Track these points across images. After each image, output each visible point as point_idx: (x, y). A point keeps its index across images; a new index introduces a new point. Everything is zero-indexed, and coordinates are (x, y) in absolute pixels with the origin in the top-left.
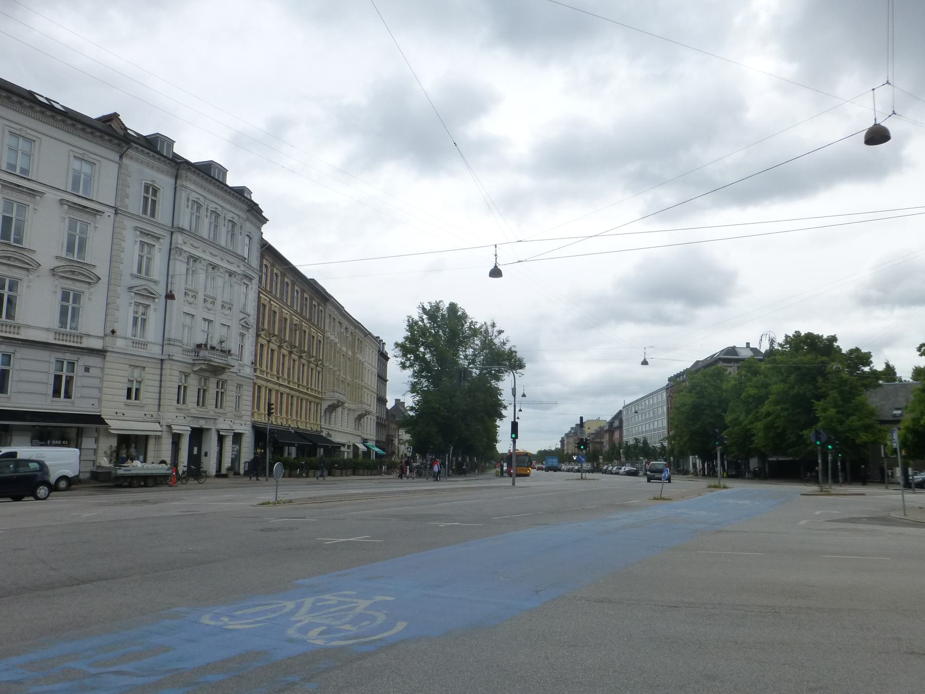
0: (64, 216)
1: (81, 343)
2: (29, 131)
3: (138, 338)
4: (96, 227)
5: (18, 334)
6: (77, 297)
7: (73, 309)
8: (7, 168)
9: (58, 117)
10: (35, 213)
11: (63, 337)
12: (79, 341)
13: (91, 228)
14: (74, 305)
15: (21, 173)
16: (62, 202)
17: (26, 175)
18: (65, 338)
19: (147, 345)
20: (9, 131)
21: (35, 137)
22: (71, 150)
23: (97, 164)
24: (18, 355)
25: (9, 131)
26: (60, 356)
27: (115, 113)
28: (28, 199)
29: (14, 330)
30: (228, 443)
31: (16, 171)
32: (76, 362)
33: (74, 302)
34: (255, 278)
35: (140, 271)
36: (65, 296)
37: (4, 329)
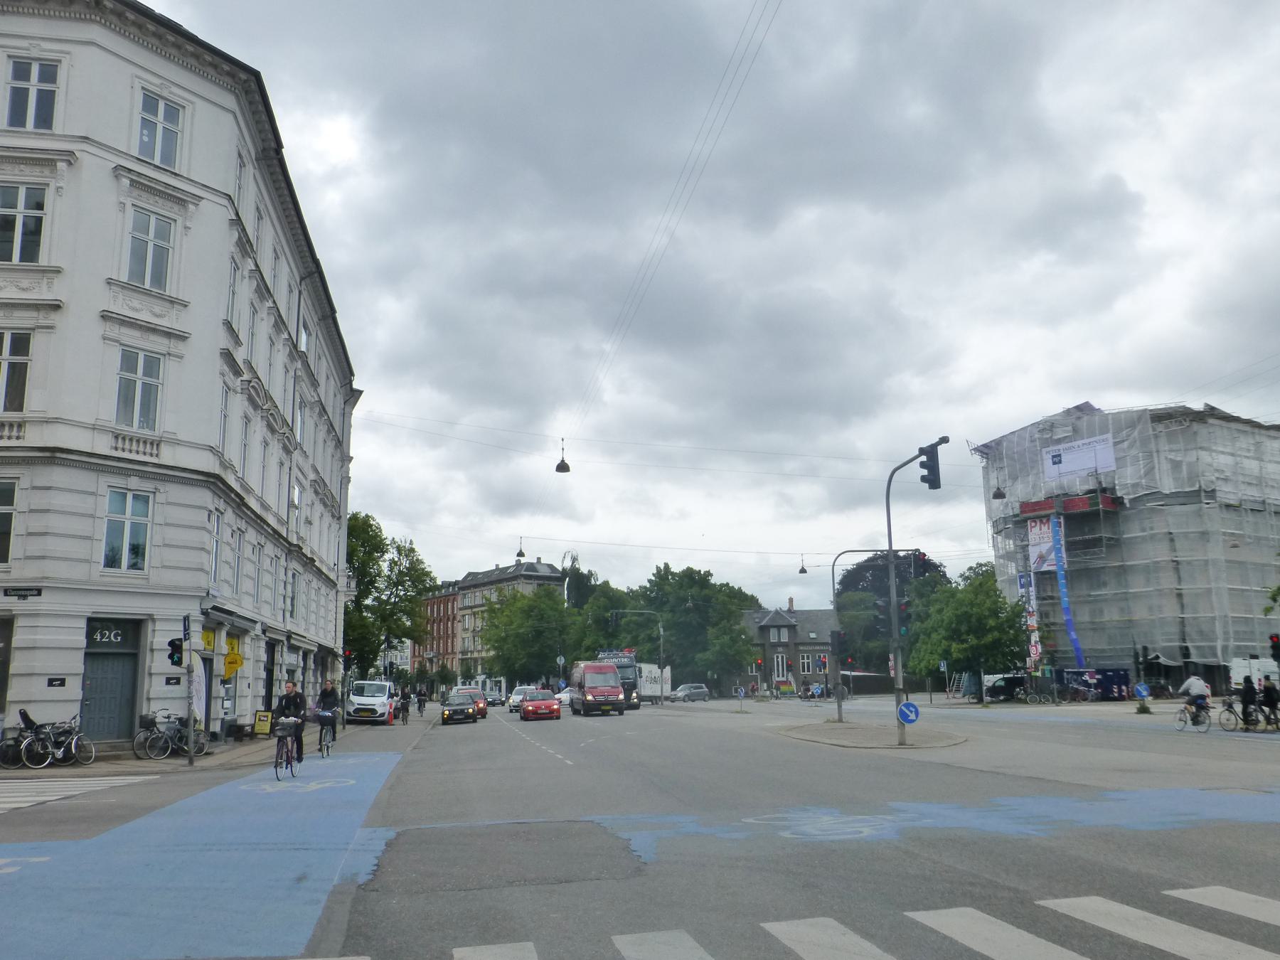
0: (122, 199)
1: (157, 456)
2: (175, 89)
3: (135, 429)
4: (186, 228)
5: (18, 438)
6: (152, 366)
7: (146, 386)
8: (139, 154)
9: (188, 47)
10: (186, 234)
11: (145, 448)
12: (155, 451)
13: (176, 230)
14: (148, 380)
15: (162, 161)
16: (118, 170)
17: (169, 166)
18: (127, 446)
19: (158, 445)
20: (143, 88)
21: (185, 100)
22: (137, 77)
23: (187, 107)
24: (160, 498)
25: (143, 88)
26: (118, 481)
27: (921, 467)
28: (176, 208)
29: (152, 449)
30: (1244, 555)
31: (153, 159)
32: (151, 496)
33: (147, 373)
34: (48, 185)
35: (136, 270)
36: (129, 360)
37: (6, 432)
